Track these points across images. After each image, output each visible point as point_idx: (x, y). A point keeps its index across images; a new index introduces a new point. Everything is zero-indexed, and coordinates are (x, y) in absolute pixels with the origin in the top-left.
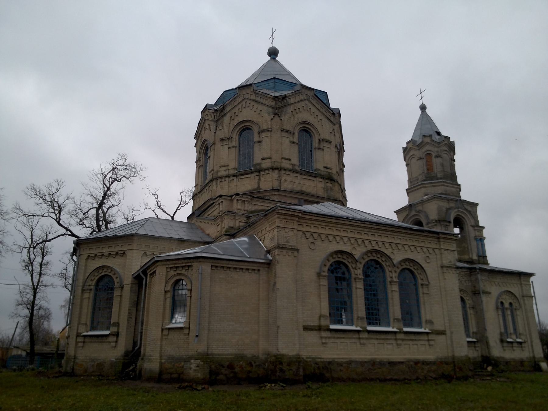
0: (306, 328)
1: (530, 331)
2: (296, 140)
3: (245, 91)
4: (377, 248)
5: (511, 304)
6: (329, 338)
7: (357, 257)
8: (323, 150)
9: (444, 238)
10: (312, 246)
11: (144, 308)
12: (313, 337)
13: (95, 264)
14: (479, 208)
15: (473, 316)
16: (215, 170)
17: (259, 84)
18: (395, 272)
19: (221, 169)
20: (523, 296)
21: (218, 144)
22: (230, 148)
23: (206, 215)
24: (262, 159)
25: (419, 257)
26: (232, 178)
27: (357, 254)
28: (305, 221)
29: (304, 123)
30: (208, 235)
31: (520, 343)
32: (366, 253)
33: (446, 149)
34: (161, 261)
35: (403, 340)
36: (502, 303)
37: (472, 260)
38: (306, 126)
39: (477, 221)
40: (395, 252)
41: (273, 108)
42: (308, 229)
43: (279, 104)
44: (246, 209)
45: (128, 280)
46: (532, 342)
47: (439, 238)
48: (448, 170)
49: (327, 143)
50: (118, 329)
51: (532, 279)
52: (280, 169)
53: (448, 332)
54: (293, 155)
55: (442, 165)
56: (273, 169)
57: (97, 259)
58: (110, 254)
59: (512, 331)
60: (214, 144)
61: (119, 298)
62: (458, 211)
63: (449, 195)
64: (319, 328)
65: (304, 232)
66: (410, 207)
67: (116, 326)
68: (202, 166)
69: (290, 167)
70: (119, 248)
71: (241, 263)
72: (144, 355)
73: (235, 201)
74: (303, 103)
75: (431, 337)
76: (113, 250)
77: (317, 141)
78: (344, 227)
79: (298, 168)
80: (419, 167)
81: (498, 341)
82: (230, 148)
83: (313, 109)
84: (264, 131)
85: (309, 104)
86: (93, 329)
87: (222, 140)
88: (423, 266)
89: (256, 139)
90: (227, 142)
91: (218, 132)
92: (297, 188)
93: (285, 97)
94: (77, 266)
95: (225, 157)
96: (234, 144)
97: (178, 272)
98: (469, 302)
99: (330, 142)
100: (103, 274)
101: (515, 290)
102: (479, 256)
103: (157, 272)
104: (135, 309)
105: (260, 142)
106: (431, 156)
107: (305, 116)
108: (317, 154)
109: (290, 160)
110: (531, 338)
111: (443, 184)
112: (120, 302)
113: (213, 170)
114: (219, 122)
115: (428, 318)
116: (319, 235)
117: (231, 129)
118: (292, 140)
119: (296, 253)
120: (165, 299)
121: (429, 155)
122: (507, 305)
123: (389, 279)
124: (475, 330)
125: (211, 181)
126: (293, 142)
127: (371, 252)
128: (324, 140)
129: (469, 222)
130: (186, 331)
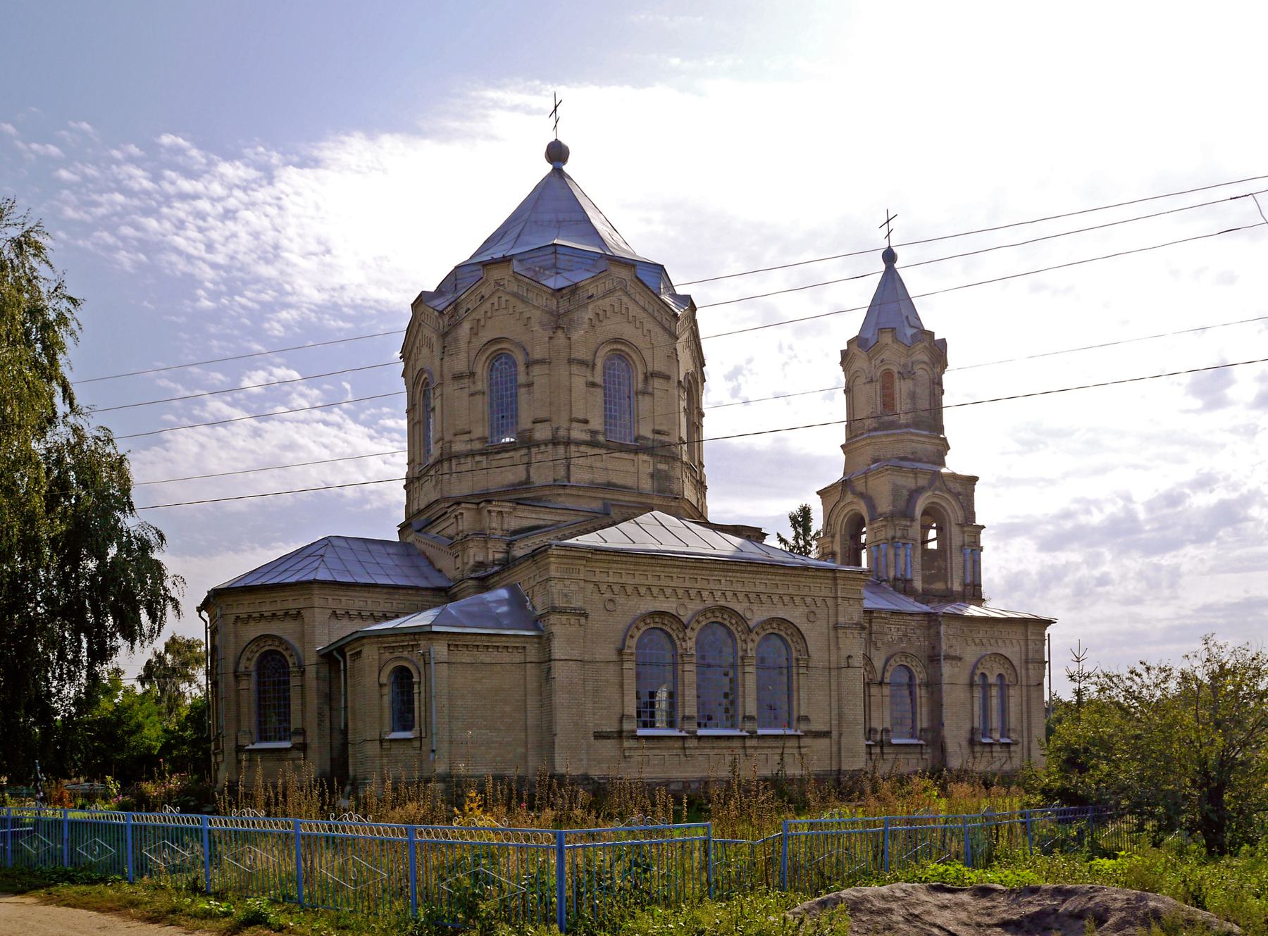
0: (599, 736)
3: (497, 273)
4: (722, 603)
5: (1000, 676)
6: (636, 749)
7: (685, 620)
8: (652, 394)
11: (346, 707)
13: (253, 631)
14: (978, 487)
16: (447, 438)
17: (527, 256)
18: (753, 641)
19: (458, 438)
22: (472, 395)
23: (434, 532)
25: (795, 615)
26: (478, 458)
27: (686, 616)
28: (598, 564)
29: (616, 341)
30: (440, 571)
31: (1008, 745)
32: (703, 613)
33: (926, 359)
34: (370, 637)
35: (755, 748)
36: (984, 675)
37: (951, 591)
38: (619, 347)
39: (970, 514)
40: (755, 607)
41: (551, 313)
42: (603, 577)
43: (564, 305)
44: (505, 526)
45: (311, 659)
48: (924, 403)
49: (662, 381)
51: (1049, 630)
53: (835, 734)
55: (913, 396)
56: (555, 442)
57: (252, 623)
58: (274, 615)
61: (299, 689)
62: (935, 495)
63: (920, 461)
64: (620, 735)
65: (596, 584)
66: (845, 485)
67: (300, 734)
68: (419, 422)
69: (585, 437)
70: (291, 605)
71: (494, 639)
72: (355, 776)
73: (485, 513)
75: (804, 742)
76: (280, 606)
77: (641, 377)
79: (601, 438)
80: (870, 395)
81: (965, 744)
82: (472, 395)
83: (634, 310)
84: (537, 362)
85: (625, 299)
86: (263, 738)
87: (457, 377)
88: (803, 629)
89: (522, 379)
90: (466, 382)
91: (446, 359)
92: (601, 478)
93: (574, 288)
94: (214, 631)
95: (466, 412)
97: (397, 654)
99: (667, 378)
100: (267, 648)
101: (1013, 651)
102: (965, 585)
103: (364, 655)
104: (326, 708)
105: (530, 385)
106: (895, 368)
109: (586, 422)
112: (303, 696)
113: (442, 439)
114: (449, 339)
115: (802, 713)
116: (623, 587)
117: (473, 354)
118: (590, 379)
119: (583, 620)
121: (888, 375)
123: (740, 654)
124: (925, 725)
125: (439, 462)
126: (593, 385)
127: (712, 610)
128: (654, 375)
130: (417, 744)
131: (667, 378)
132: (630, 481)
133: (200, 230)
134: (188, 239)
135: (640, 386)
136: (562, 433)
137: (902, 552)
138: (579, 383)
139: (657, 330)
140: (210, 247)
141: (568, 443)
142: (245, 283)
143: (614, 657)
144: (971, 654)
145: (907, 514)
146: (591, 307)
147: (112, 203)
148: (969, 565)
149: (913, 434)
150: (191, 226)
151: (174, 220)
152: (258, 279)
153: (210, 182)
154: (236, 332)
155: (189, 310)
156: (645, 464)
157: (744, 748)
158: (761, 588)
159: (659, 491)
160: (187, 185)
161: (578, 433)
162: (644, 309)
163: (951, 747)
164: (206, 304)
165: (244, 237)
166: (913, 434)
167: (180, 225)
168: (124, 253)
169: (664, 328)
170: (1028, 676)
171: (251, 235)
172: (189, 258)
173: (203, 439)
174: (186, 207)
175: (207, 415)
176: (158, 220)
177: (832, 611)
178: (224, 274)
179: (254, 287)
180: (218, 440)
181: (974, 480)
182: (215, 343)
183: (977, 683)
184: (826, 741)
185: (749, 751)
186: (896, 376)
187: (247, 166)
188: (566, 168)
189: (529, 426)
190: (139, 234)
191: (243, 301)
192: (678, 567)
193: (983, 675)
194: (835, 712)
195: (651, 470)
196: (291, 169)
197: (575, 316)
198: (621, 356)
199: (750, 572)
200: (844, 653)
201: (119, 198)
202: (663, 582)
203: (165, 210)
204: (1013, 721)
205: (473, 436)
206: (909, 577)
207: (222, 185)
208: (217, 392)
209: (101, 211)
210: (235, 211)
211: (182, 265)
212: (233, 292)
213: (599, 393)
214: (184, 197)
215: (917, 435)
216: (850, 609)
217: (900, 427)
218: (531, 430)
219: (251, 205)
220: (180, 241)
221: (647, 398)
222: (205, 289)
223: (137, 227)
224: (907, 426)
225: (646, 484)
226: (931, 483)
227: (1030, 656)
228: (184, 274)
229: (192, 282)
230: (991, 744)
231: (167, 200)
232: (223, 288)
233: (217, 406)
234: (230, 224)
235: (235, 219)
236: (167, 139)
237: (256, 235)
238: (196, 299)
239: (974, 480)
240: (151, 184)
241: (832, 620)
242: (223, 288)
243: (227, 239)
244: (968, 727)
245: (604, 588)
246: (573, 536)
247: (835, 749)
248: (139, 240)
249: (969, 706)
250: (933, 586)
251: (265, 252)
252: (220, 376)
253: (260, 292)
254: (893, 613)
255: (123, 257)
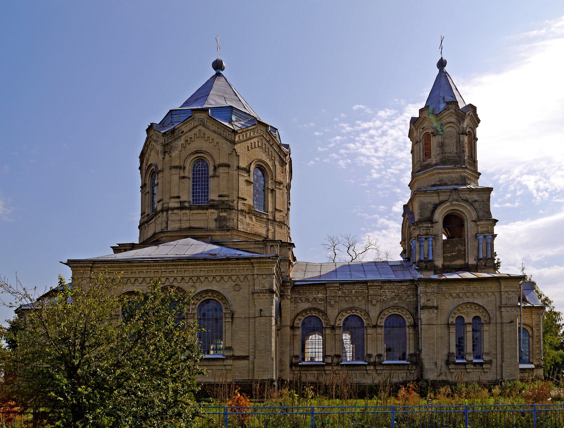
8: (218, 176)
14: (493, 194)
15: (411, 335)
21: (167, 172)
29: (196, 152)
33: (453, 120)
38: (200, 155)
47: (252, 263)
49: (224, 168)
53: (251, 358)
60: (162, 171)
74: (196, 130)
78: (139, 268)
85: (203, 129)
92: (185, 225)
93: (173, 131)
98: (409, 321)
99: (228, 166)
108: (212, 183)
111: (437, 171)
118: (182, 175)
124: (412, 352)
131: (228, 166)
132: (202, 225)
133: (372, 143)
134: (366, 149)
137: (425, 244)
138: (175, 178)
139: (222, 141)
140: (376, 150)
141: (167, 210)
142: (392, 162)
144: (448, 304)
145: (430, 220)
146: (183, 137)
147: (336, 141)
149: (440, 169)
150: (368, 143)
151: (361, 141)
152: (397, 160)
153: (375, 121)
154: (389, 186)
155: (369, 180)
156: (213, 214)
159: (220, 228)
160: (365, 125)
161: (174, 204)
162: (214, 132)
164: (376, 176)
165: (391, 142)
166: (440, 169)
167: (363, 143)
168: (341, 161)
169: (227, 140)
170: (502, 317)
171: (393, 140)
172: (368, 157)
173: (377, 237)
174: (365, 135)
175: (378, 226)
176: (354, 144)
178: (383, 161)
179: (396, 163)
180: (384, 236)
181: (490, 190)
182: (380, 192)
184: (245, 362)
185: (369, 372)
186: (431, 135)
187: (390, 109)
190: (348, 152)
191: (391, 171)
192: (145, 266)
194: (252, 344)
195: (216, 217)
196: (410, 105)
197: (174, 144)
198: (201, 159)
200: (258, 308)
201: (338, 138)
203: (357, 139)
204: (486, 347)
206: (431, 258)
207: (380, 121)
208: (382, 215)
209: (332, 145)
210: (386, 131)
211: (365, 161)
212: (387, 167)
214: (365, 130)
215: (443, 169)
216: (263, 281)
217: (432, 166)
219: (392, 127)
220: (363, 151)
221: (216, 179)
222: (375, 169)
223: (347, 149)
224: (436, 164)
225: (213, 225)
227: (503, 302)
228: (366, 164)
229: (369, 167)
230: (464, 364)
231: (357, 134)
232: (383, 167)
233: (383, 221)
234: (384, 138)
235: (386, 135)
236: (356, 107)
237: (396, 139)
238: (371, 174)
239: (490, 190)
240: (351, 129)
241: (251, 288)
242: (383, 167)
243: (383, 144)
244: (445, 352)
246: (453, 261)
247: (251, 366)
248: (346, 154)
249: (446, 338)
250: (454, 263)
251: (401, 146)
252: (382, 207)
253: (399, 165)
254: (384, 282)
255: (341, 163)
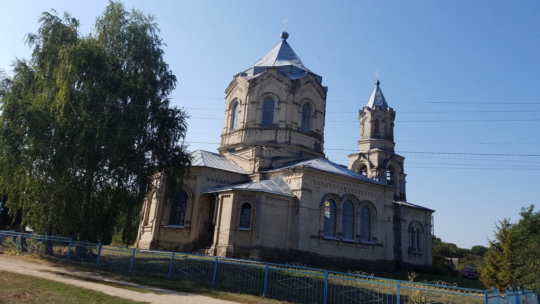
0: (312, 237)
1: (427, 247)
2: (301, 111)
9: (388, 189)
10: (318, 189)
12: (315, 242)
20: (426, 225)
24: (280, 121)
25: (373, 200)
26: (257, 131)
29: (308, 99)
31: (420, 255)
39: (402, 170)
46: (427, 255)
48: (388, 131)
50: (190, 225)
51: (433, 214)
52: (291, 130)
54: (298, 119)
55: (385, 128)
59: (416, 247)
64: (319, 237)
79: (301, 130)
84: (282, 102)
85: (312, 86)
89: (276, 106)
96: (260, 107)
101: (422, 220)
102: (400, 194)
105: (279, 109)
107: (308, 94)
109: (297, 124)
110: (427, 252)
117: (259, 97)
120: (237, 213)
122: (415, 230)
129: (398, 169)
135: (313, 115)
136: (289, 126)
141: (291, 130)
143: (318, 208)
144: (409, 220)
148: (402, 187)
157: (356, 247)
158: (363, 190)
161: (294, 128)
163: (403, 254)
177: (384, 200)
183: (411, 230)
188: (287, 40)
189: (277, 122)
193: (412, 228)
199: (361, 183)
202: (335, 183)
204: (422, 246)
205: (256, 123)
213: (301, 114)
218: (278, 124)
221: (315, 119)
226: (391, 158)
241: (384, 204)
245: (317, 183)
